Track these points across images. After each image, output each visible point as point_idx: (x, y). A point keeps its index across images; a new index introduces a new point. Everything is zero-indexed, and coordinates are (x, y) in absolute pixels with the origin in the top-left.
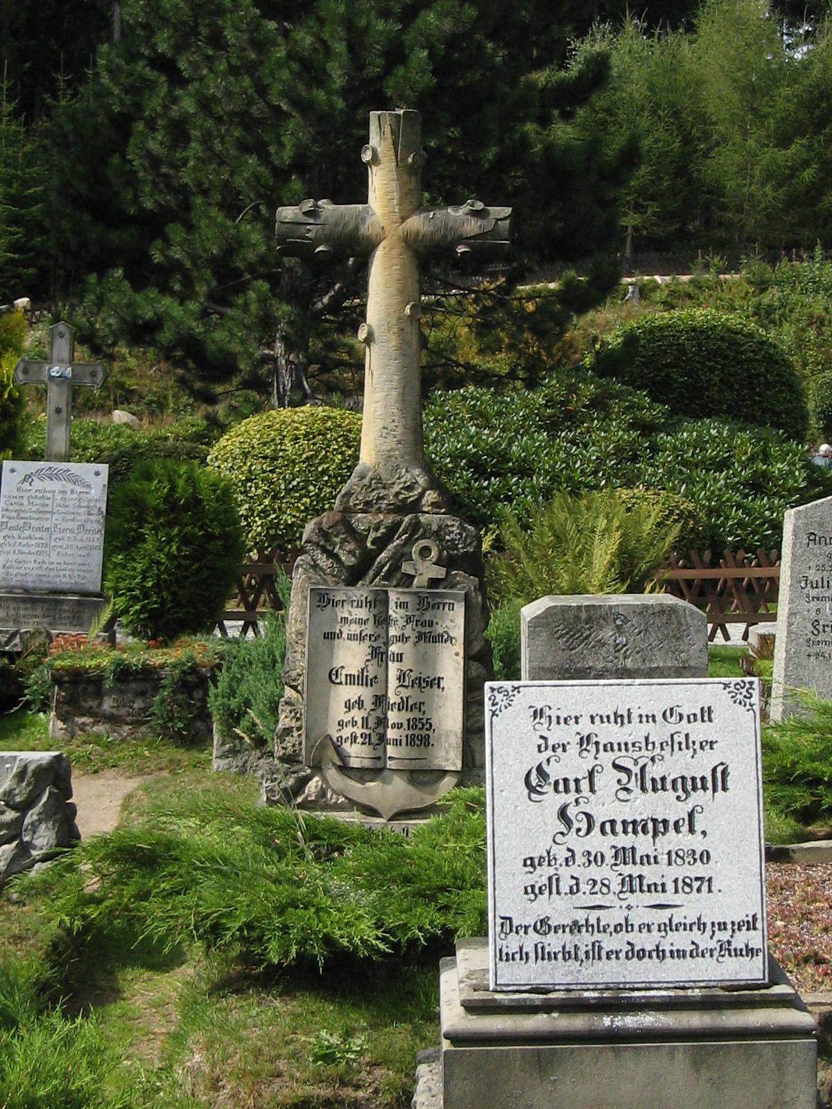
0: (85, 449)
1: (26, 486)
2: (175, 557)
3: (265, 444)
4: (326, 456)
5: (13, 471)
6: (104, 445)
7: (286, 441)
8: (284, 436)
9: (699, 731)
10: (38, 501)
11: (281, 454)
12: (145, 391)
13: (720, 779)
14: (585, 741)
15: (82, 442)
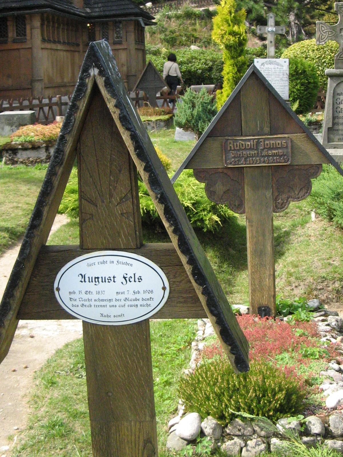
0: (200, 60)
1: (262, 67)
2: (299, 90)
3: (302, 53)
4: (325, 57)
5: (258, 62)
6: (208, 58)
7: (310, 51)
8: (309, 50)
10: (267, 72)
11: (309, 56)
12: (202, 37)
15: (199, 57)
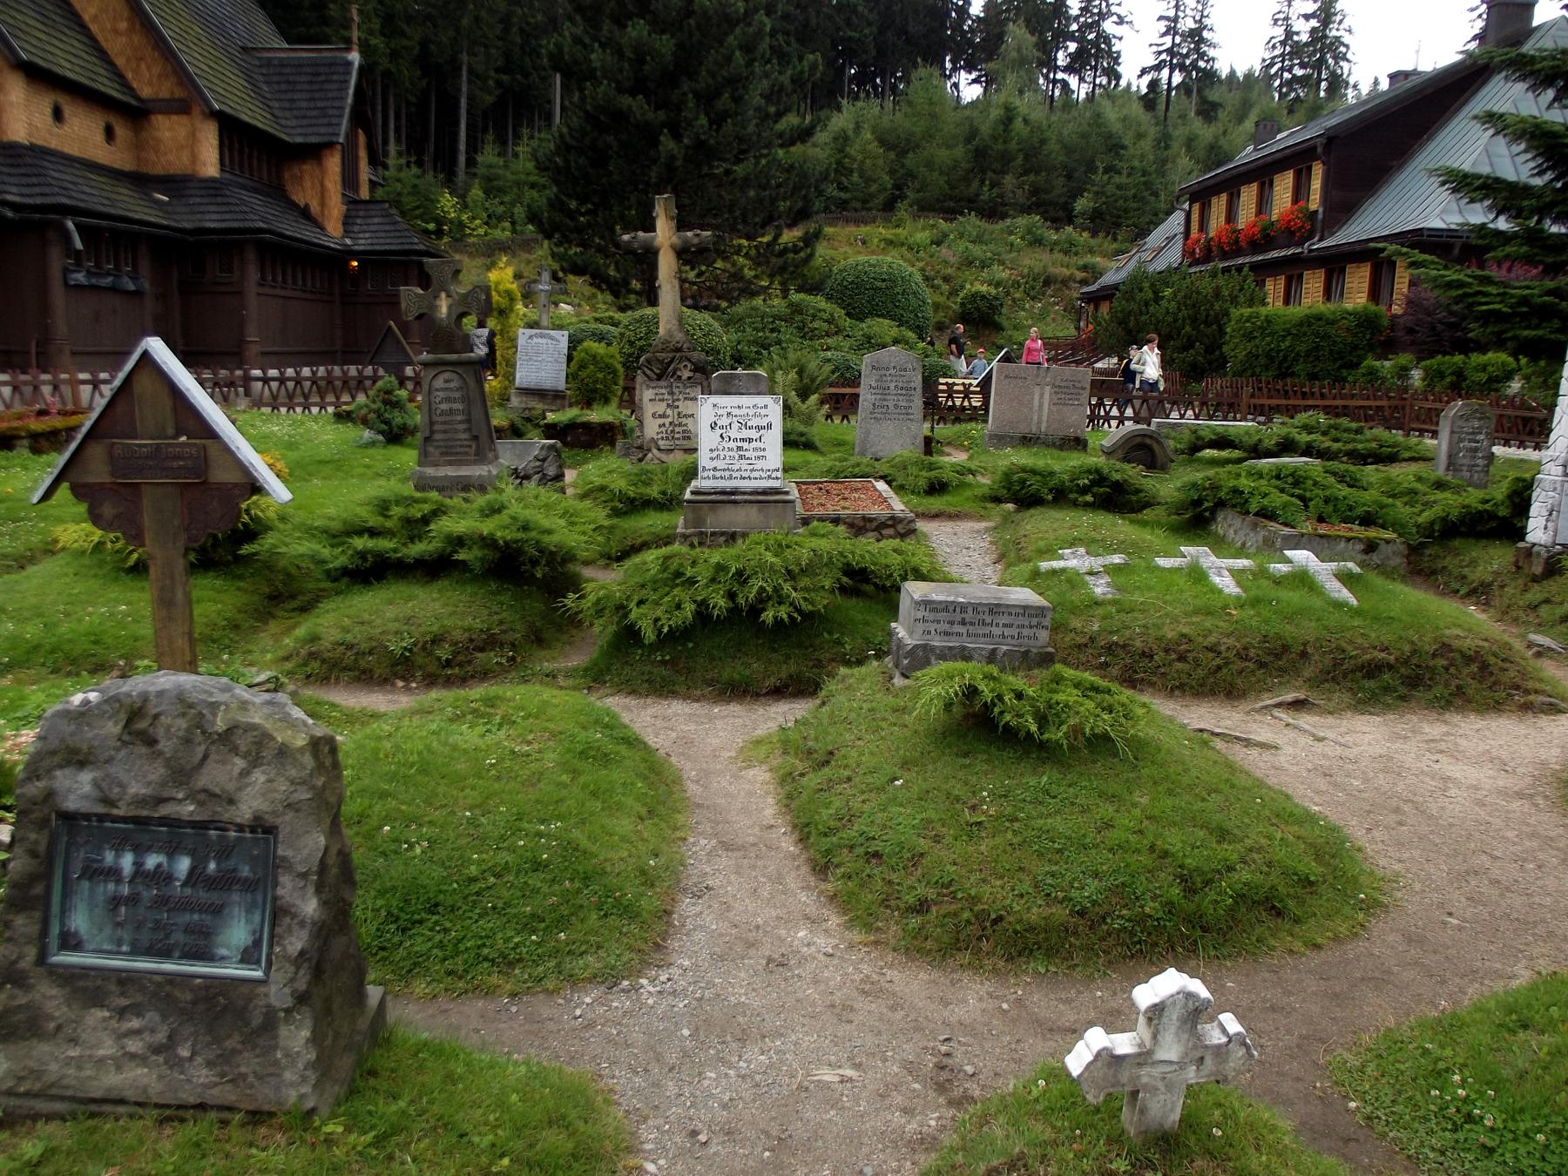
9: (763, 412)
13: (769, 426)
14: (729, 414)
